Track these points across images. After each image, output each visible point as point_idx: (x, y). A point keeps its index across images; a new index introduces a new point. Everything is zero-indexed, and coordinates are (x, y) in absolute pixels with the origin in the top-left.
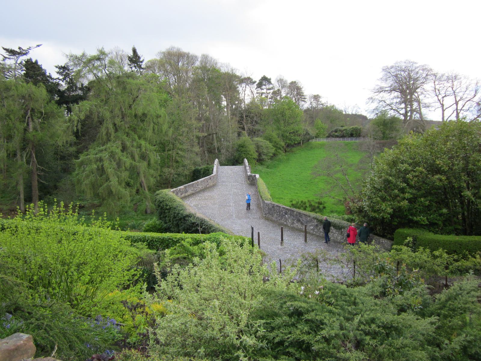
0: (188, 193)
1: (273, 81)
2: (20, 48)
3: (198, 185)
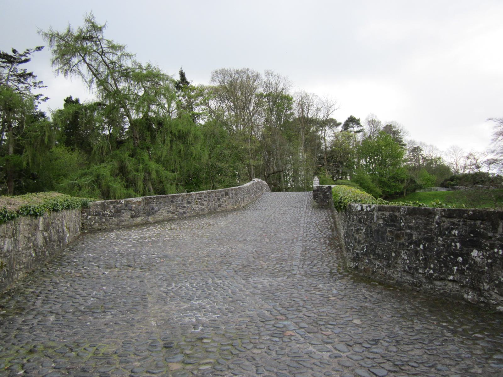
0: (158, 217)
1: (362, 122)
2: (14, 51)
3: (189, 203)
